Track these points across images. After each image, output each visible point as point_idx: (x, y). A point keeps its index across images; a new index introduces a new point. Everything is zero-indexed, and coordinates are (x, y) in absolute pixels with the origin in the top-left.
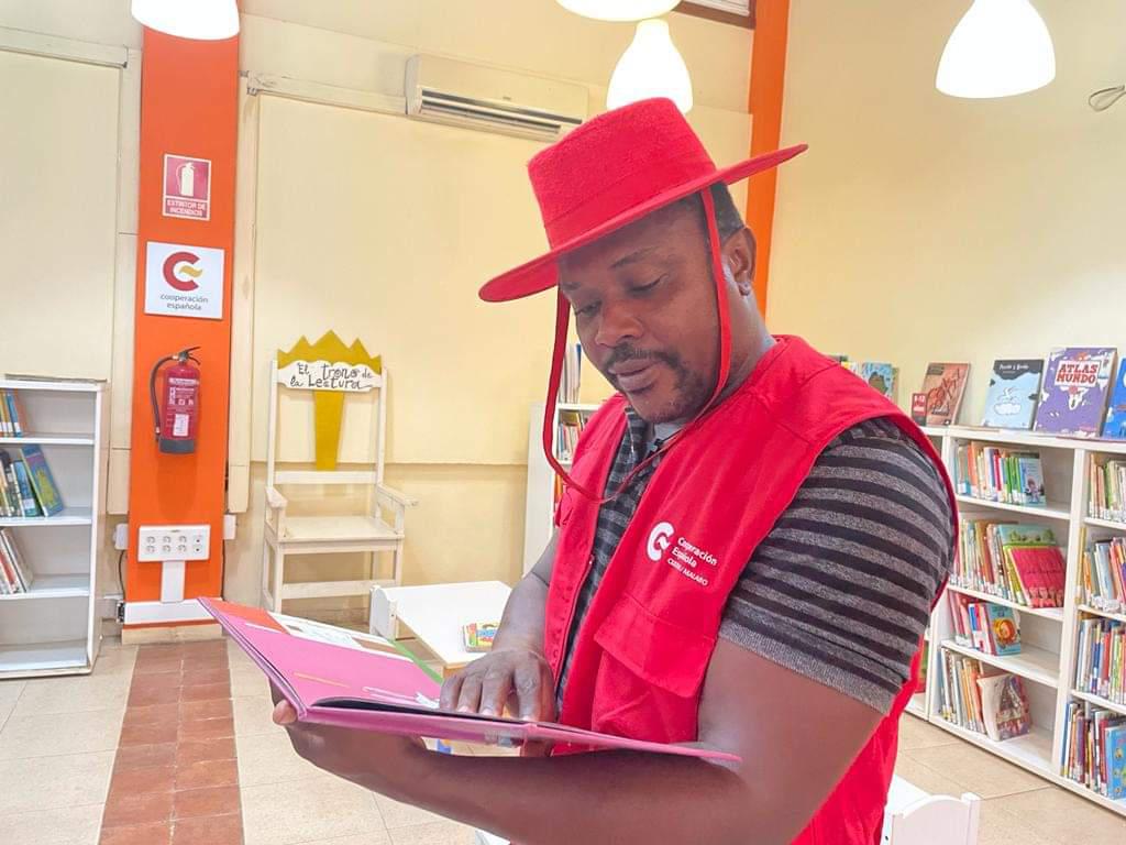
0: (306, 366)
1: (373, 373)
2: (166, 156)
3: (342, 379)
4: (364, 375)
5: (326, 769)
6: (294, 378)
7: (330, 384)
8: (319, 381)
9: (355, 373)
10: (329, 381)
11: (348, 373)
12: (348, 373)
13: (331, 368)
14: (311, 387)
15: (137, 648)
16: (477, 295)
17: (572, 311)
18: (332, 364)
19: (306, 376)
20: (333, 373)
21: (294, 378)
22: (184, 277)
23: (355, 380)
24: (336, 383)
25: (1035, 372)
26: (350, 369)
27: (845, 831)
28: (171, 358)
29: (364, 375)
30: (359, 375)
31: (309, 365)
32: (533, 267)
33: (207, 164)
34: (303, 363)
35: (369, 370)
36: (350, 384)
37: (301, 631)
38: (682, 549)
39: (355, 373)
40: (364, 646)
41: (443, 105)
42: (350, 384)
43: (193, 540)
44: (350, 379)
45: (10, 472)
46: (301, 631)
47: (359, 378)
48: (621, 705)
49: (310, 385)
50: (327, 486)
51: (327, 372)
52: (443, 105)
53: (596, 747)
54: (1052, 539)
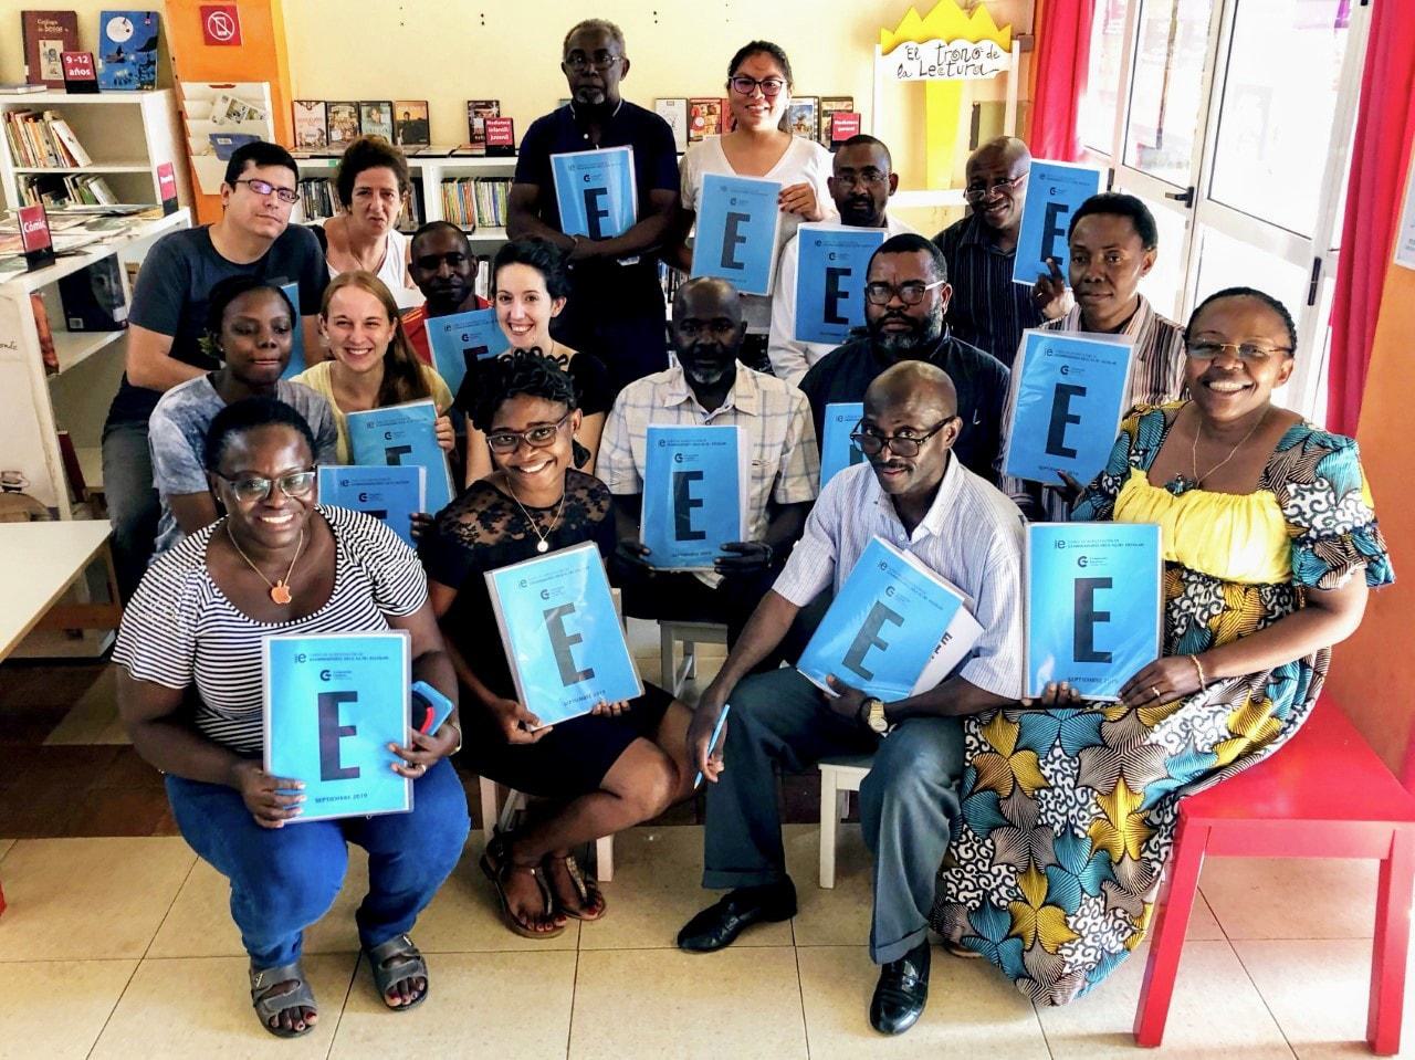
1: (1001, 52)
2: (553, 157)
4: (989, 55)
6: (901, 66)
7: (945, 71)
10: (945, 67)
11: (969, 55)
13: (947, 49)
14: (923, 77)
16: (589, 17)
19: (916, 64)
21: (901, 66)
23: (978, 63)
25: (315, 313)
27: (994, 329)
29: (989, 55)
30: (983, 55)
31: (920, 47)
37: (212, 86)
38: (492, 126)
41: (1142, 545)
42: (971, 69)
46: (212, 86)
47: (983, 60)
51: (942, 55)
52: (1142, 545)
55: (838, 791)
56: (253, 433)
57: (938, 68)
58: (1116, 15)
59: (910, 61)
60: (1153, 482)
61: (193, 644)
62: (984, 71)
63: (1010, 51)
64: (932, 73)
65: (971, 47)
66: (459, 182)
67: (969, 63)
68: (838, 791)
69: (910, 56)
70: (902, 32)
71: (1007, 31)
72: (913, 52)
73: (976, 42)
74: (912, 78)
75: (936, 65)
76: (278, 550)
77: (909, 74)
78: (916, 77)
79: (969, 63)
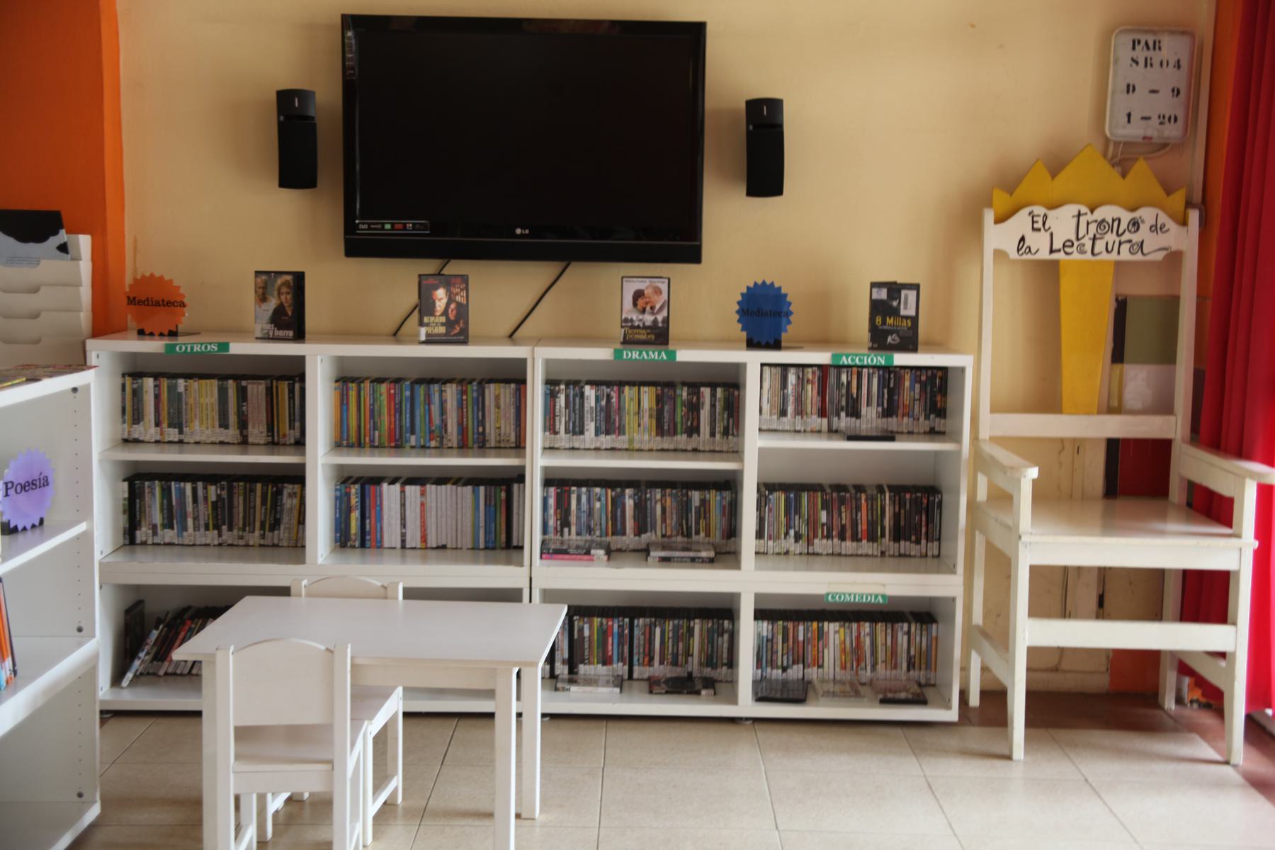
0: (1045, 216)
1: (1171, 224)
3: (1111, 237)
4: (1154, 228)
6: (1023, 239)
8: (1068, 244)
9: (1135, 224)
11: (1123, 226)
12: (1123, 226)
13: (1090, 217)
14: (1055, 256)
17: (175, 521)
18: (1092, 212)
19: (1044, 236)
20: (1093, 227)
21: (1023, 239)
23: (1136, 238)
24: (1100, 246)
26: (1126, 217)
29: (1154, 228)
30: (1144, 228)
31: (1051, 214)
34: (1040, 210)
35: (1163, 218)
36: (1125, 247)
39: (1135, 224)
40: (352, 780)
44: (1127, 236)
45: (370, 405)
47: (1143, 233)
48: (267, 338)
49: (1052, 251)
50: (760, 534)
53: (336, 532)
54: (890, 556)
55: (1234, 624)
56: (367, 534)
57: (1076, 244)
58: (885, 387)
59: (1036, 234)
60: (802, 697)
61: (785, 664)
62: (1145, 251)
63: (1184, 223)
64: (1068, 250)
65: (1126, 217)
67: (1124, 238)
68: (1234, 624)
69: (1036, 226)
70: (1021, 192)
71: (1178, 199)
72: (1040, 220)
73: (1133, 209)
74: (1037, 257)
75: (1073, 238)
76: (455, 722)
77: (1033, 250)
78: (1044, 255)
79: (1124, 238)
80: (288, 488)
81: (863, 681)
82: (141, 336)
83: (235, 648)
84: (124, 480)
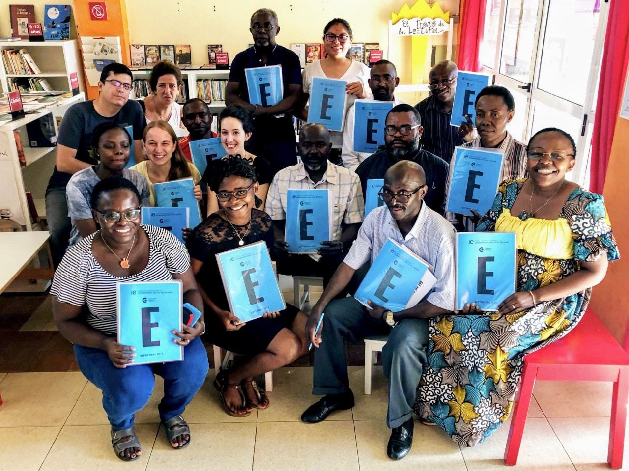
1: (445, 23)
4: (440, 24)
5: (355, 142)
6: (401, 29)
7: (420, 31)
10: (420, 30)
11: (431, 24)
13: (421, 22)
14: (410, 34)
15: (279, 275)
19: (407, 28)
21: (401, 29)
22: (481, 250)
23: (435, 28)
24: (424, 31)
28: (238, 389)
29: (440, 24)
30: (437, 24)
31: (409, 21)
32: (611, 37)
33: (178, 284)
35: (443, 22)
37: (94, 38)
42: (432, 31)
43: (574, 271)
46: (94, 38)
47: (437, 27)
51: (419, 24)
55: (373, 352)
56: (112, 192)
57: (417, 30)
59: (405, 27)
62: (437, 32)
63: (449, 23)
64: (414, 32)
65: (432, 21)
66: (204, 81)
67: (431, 28)
68: (373, 352)
72: (406, 23)
73: (434, 19)
74: (405, 35)
75: (416, 29)
77: (404, 33)
78: (407, 34)
79: (431, 28)
80: (376, 363)
81: (542, 317)
82: (71, 19)
83: (317, 348)
84: (287, 304)
